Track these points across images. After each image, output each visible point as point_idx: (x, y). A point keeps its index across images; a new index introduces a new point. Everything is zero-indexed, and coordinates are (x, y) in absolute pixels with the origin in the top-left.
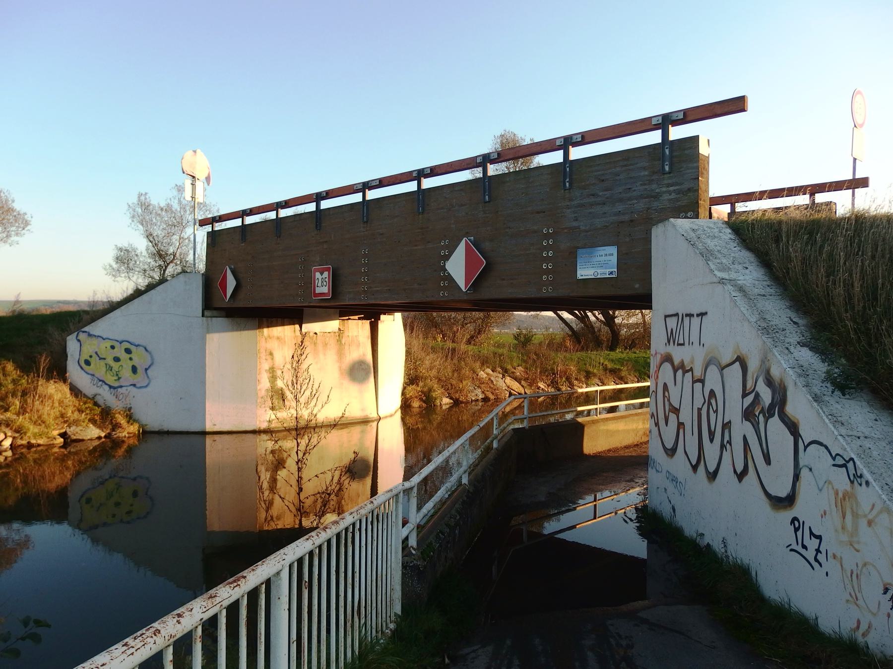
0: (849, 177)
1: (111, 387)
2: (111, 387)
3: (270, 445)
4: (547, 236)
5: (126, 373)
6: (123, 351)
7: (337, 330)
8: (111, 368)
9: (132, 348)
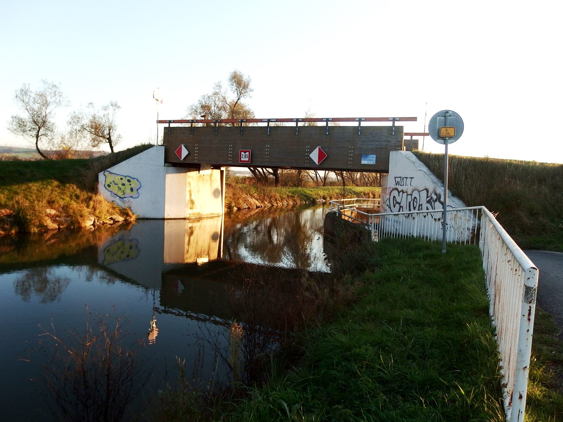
0: (423, 132)
1: (120, 197)
2: (120, 197)
3: (190, 225)
4: (351, 149)
5: (128, 191)
6: (127, 181)
7: (210, 174)
8: (120, 189)
9: (131, 180)
